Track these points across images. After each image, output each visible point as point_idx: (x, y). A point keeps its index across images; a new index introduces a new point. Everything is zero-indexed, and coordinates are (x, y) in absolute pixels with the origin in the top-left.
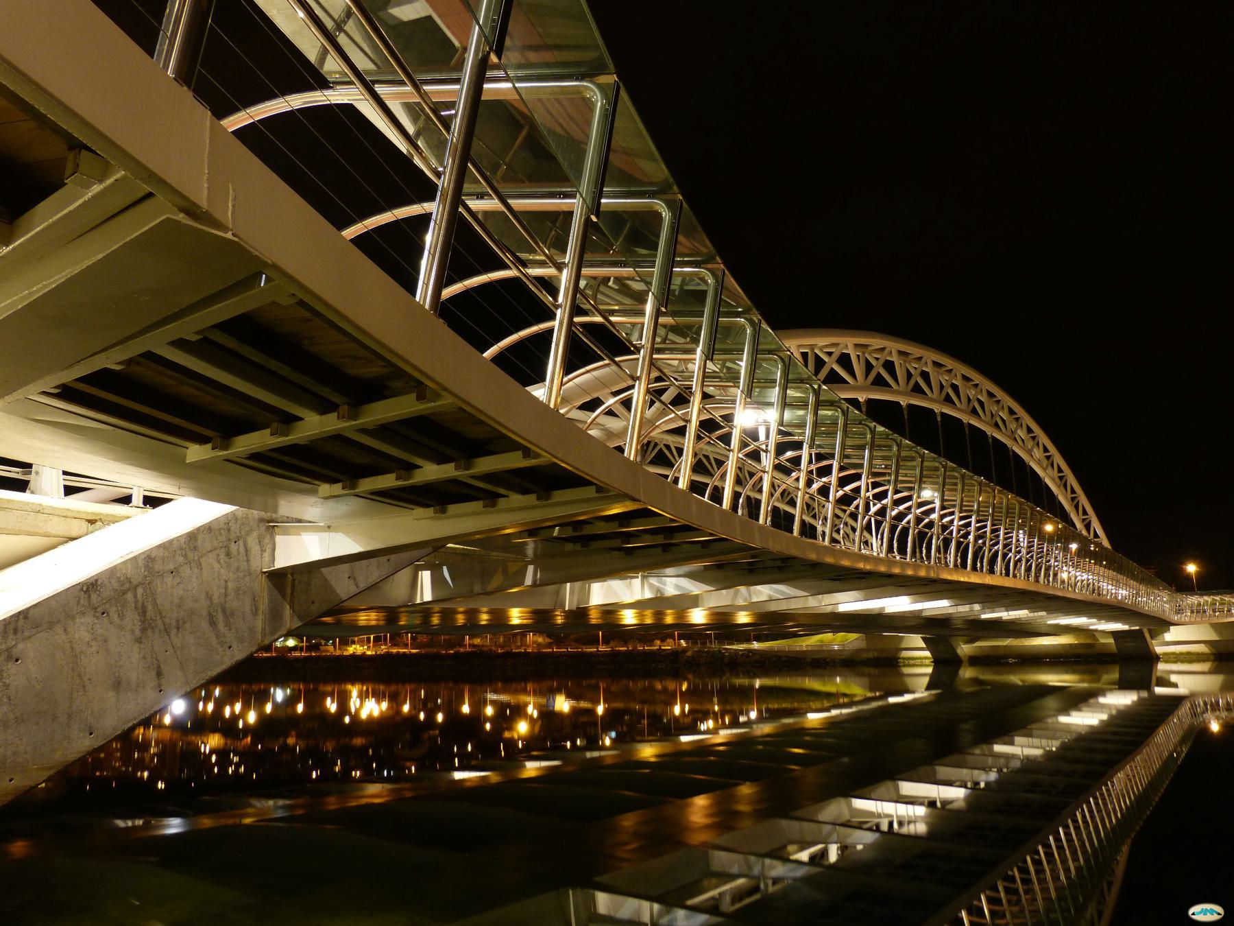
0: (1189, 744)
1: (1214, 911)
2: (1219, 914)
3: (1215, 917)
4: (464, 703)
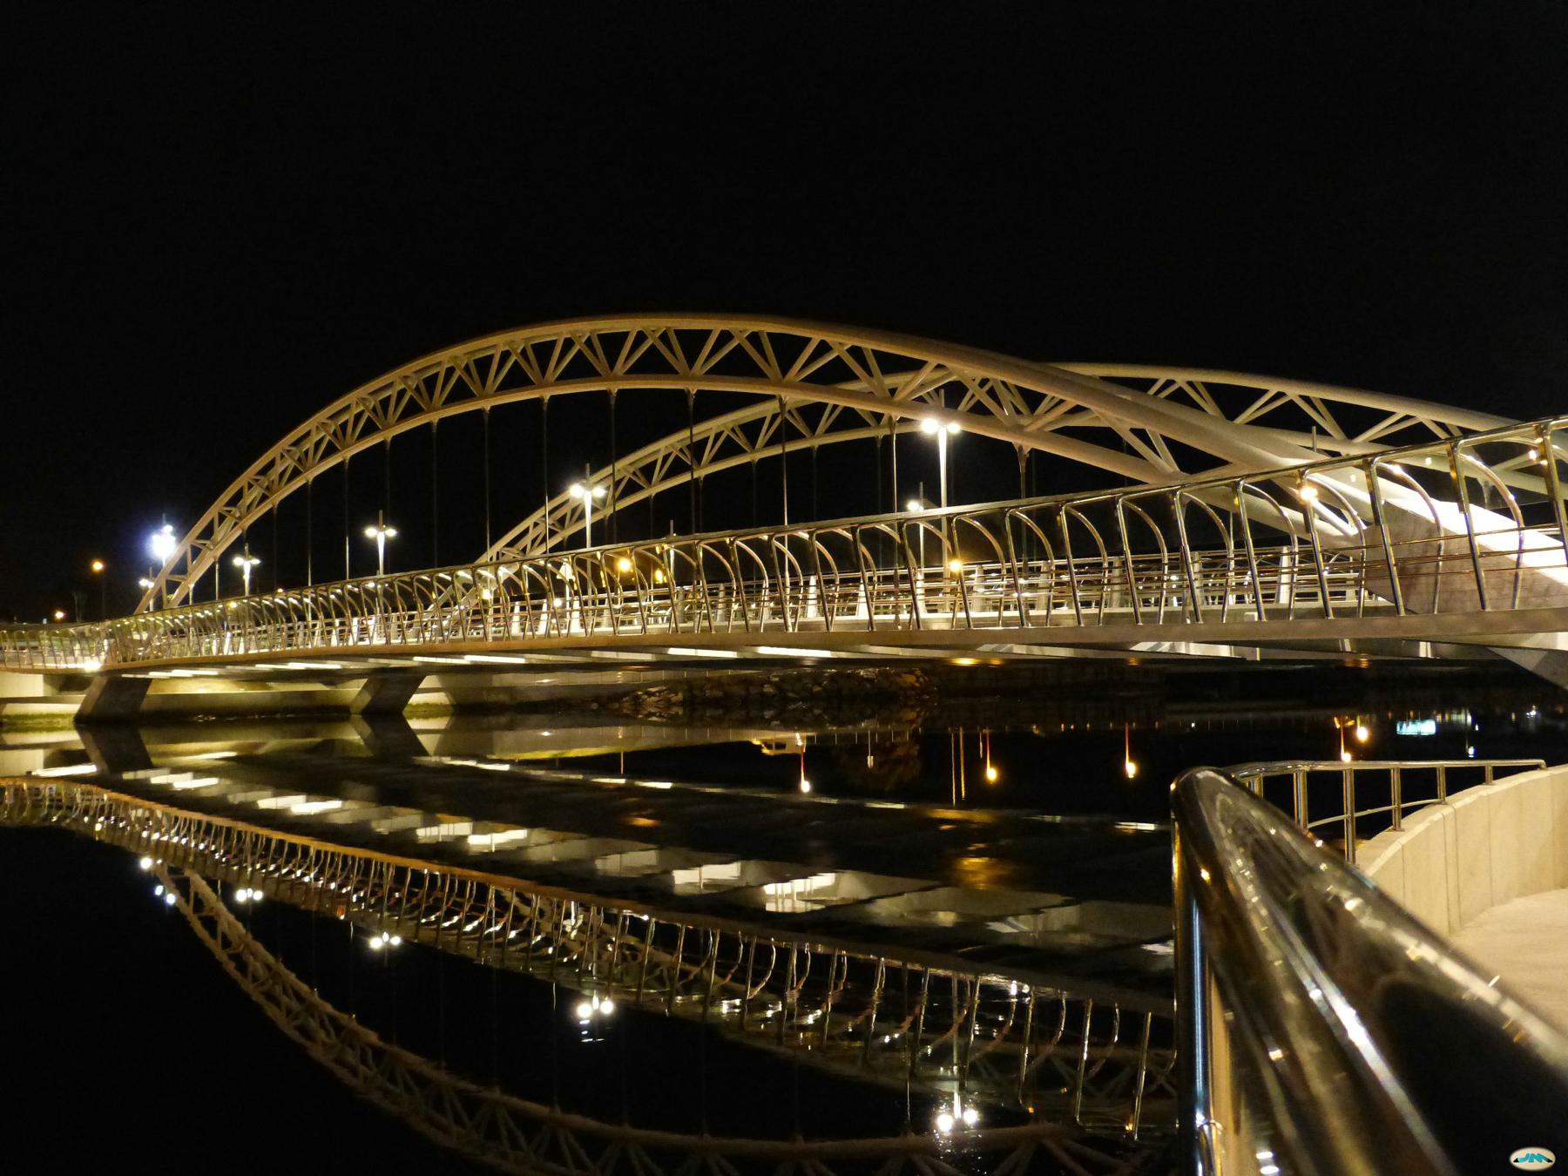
0: (1320, 1005)
1: (1543, 1157)
2: (1549, 1161)
3: (1544, 1165)
4: (147, 780)
